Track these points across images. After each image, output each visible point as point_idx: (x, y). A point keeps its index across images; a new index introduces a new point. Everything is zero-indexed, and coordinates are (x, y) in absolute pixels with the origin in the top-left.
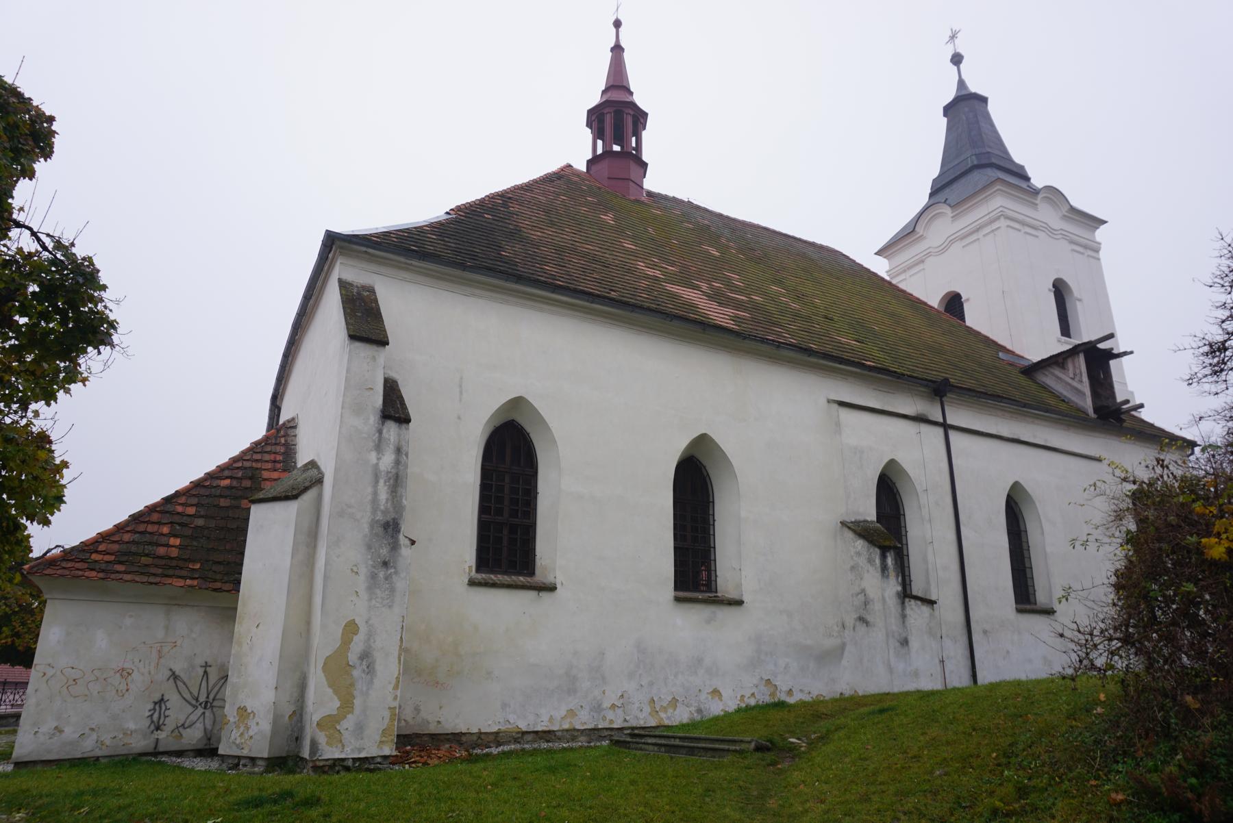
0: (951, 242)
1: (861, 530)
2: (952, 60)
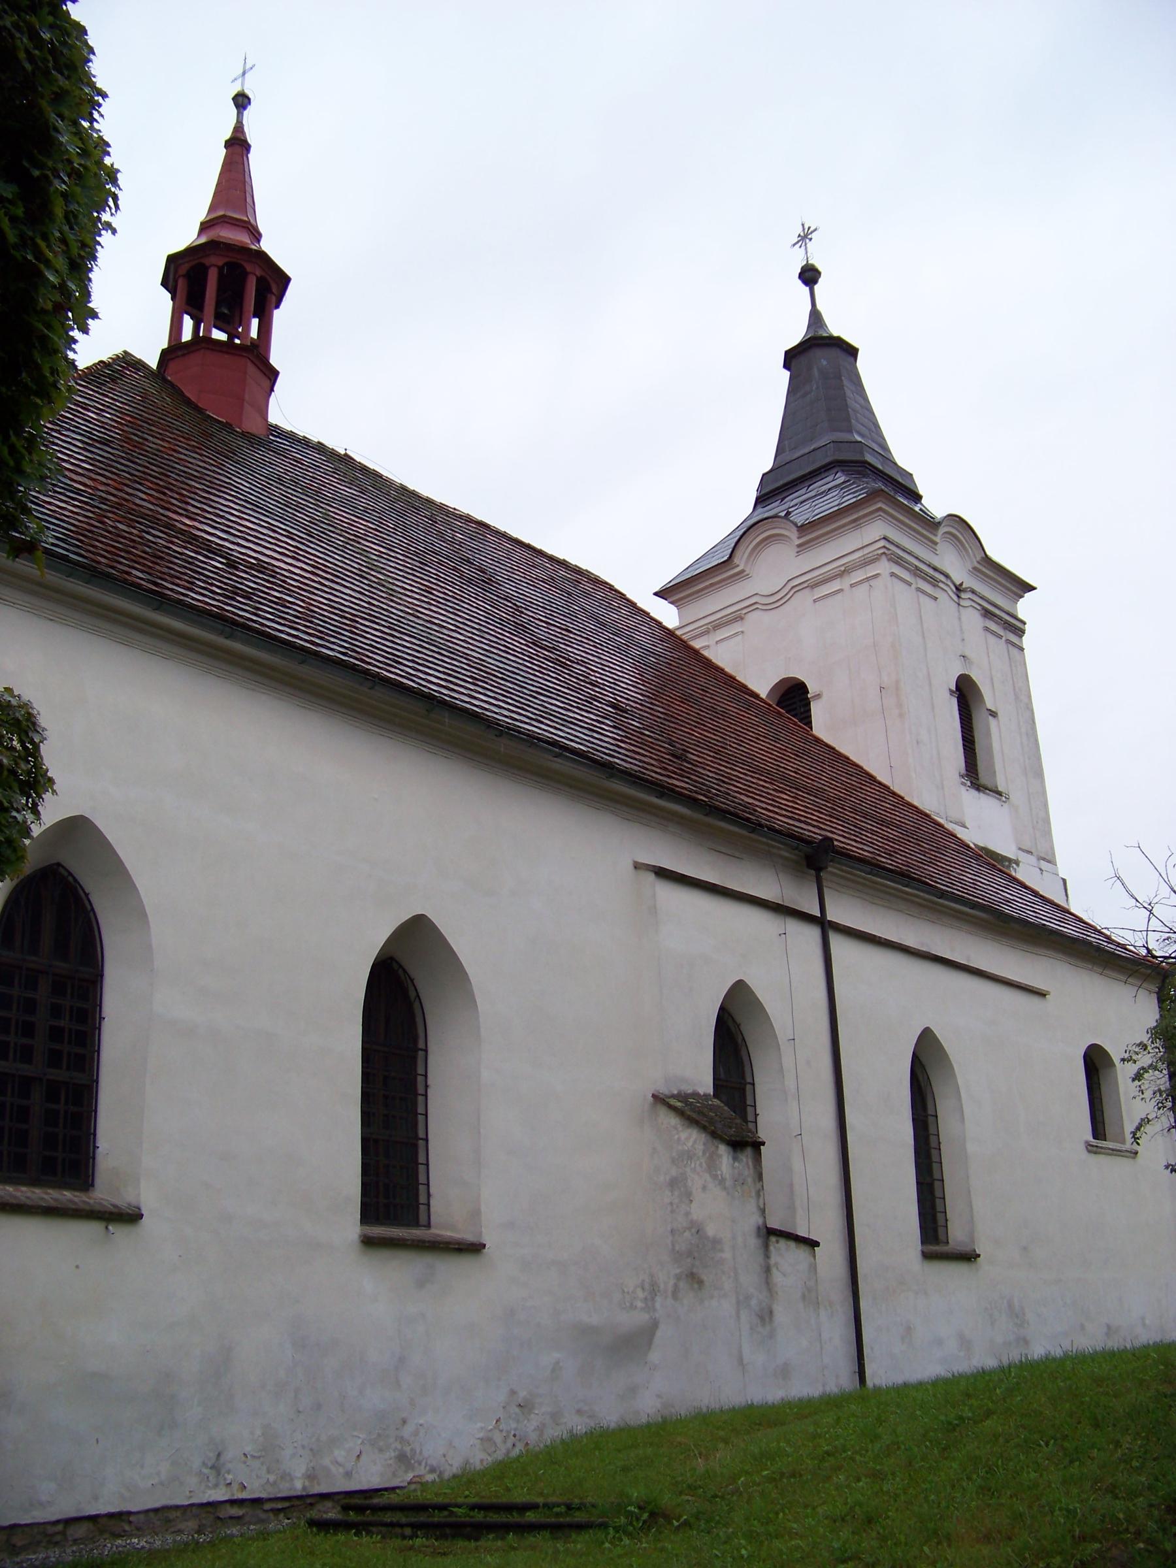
0: (795, 588)
1: (683, 1107)
2: (801, 276)
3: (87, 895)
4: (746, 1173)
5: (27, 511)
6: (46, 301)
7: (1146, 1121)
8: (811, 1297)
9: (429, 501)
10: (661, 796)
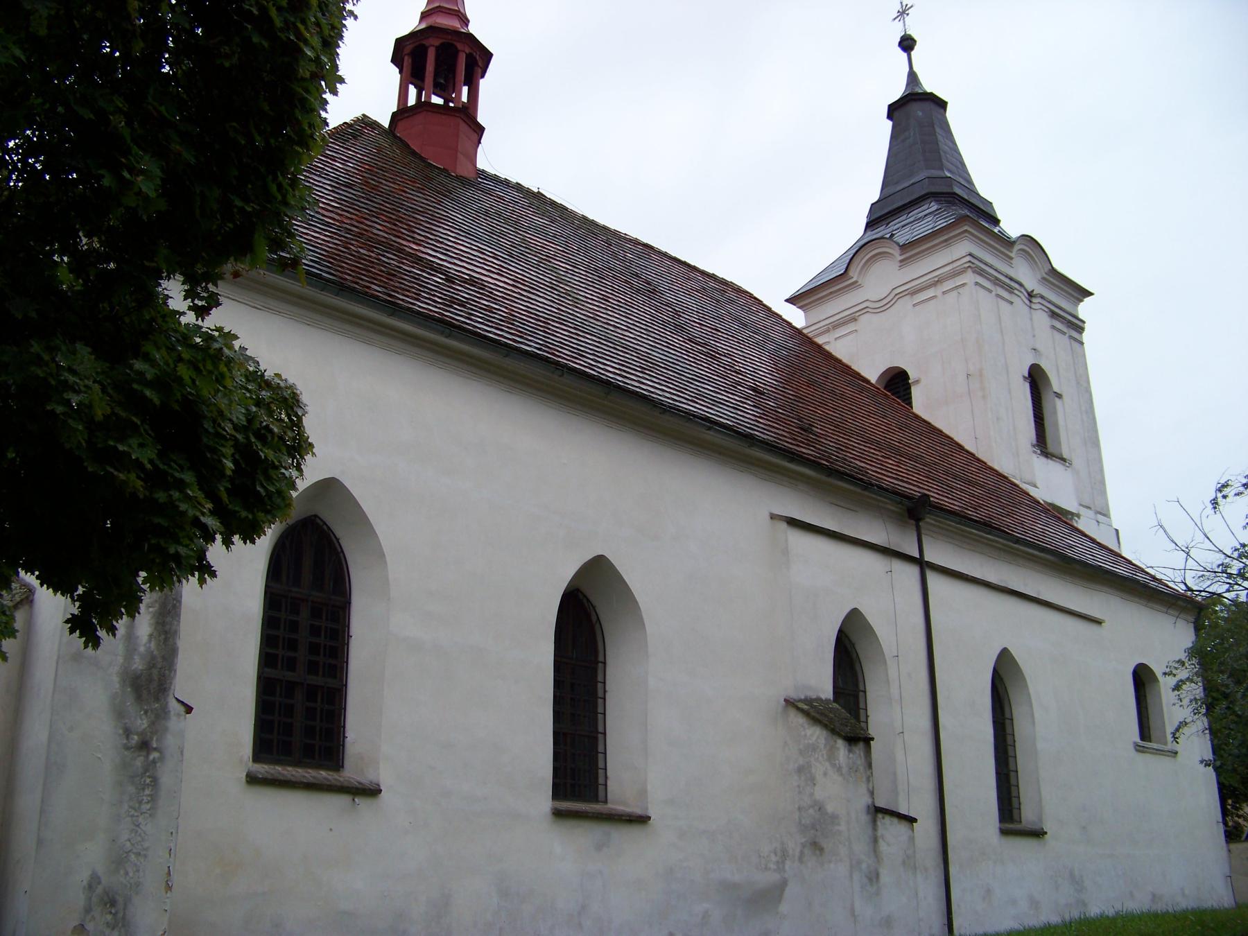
1: (810, 710)
2: (900, 44)
3: (338, 540)
4: (859, 762)
5: (291, 235)
6: (304, 71)
7: (1183, 724)
8: (909, 862)
9: (605, 228)
10: (792, 460)
